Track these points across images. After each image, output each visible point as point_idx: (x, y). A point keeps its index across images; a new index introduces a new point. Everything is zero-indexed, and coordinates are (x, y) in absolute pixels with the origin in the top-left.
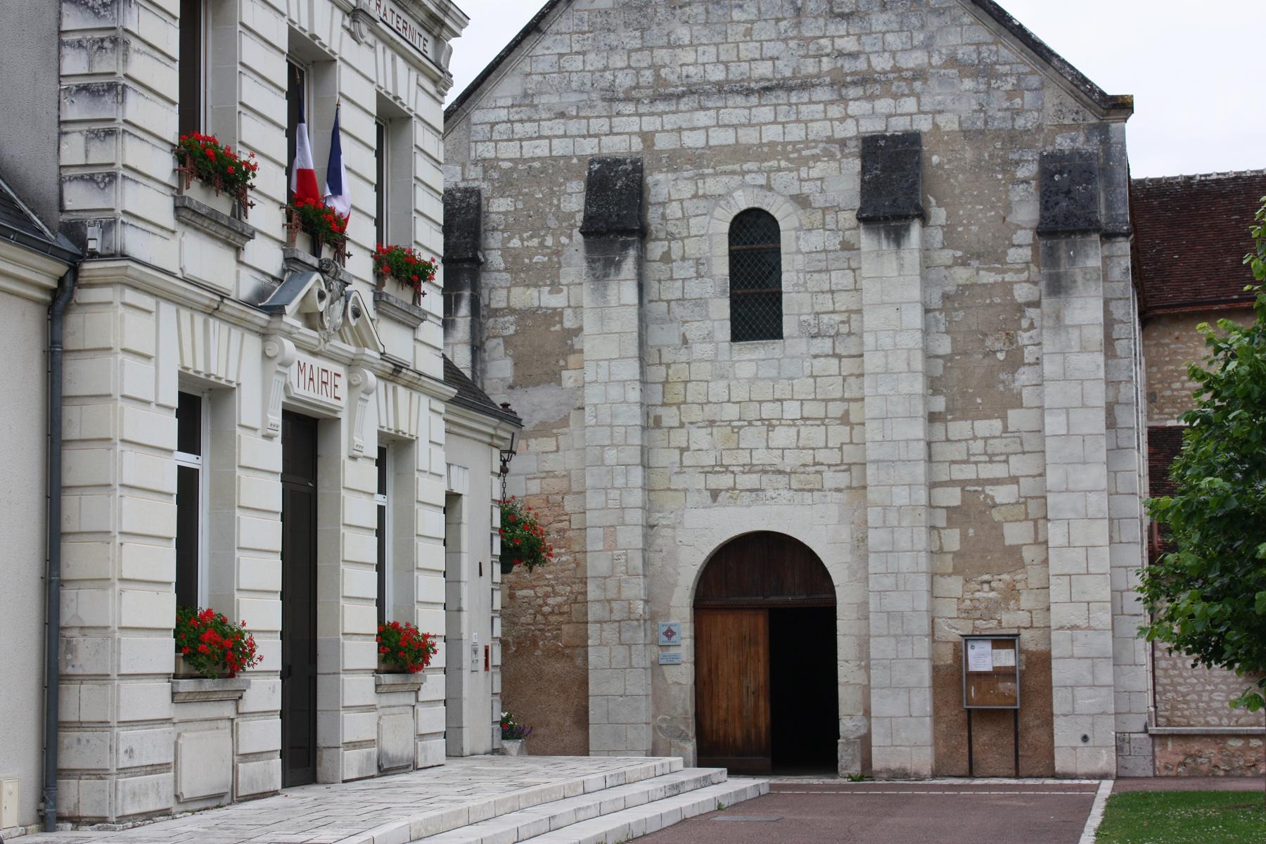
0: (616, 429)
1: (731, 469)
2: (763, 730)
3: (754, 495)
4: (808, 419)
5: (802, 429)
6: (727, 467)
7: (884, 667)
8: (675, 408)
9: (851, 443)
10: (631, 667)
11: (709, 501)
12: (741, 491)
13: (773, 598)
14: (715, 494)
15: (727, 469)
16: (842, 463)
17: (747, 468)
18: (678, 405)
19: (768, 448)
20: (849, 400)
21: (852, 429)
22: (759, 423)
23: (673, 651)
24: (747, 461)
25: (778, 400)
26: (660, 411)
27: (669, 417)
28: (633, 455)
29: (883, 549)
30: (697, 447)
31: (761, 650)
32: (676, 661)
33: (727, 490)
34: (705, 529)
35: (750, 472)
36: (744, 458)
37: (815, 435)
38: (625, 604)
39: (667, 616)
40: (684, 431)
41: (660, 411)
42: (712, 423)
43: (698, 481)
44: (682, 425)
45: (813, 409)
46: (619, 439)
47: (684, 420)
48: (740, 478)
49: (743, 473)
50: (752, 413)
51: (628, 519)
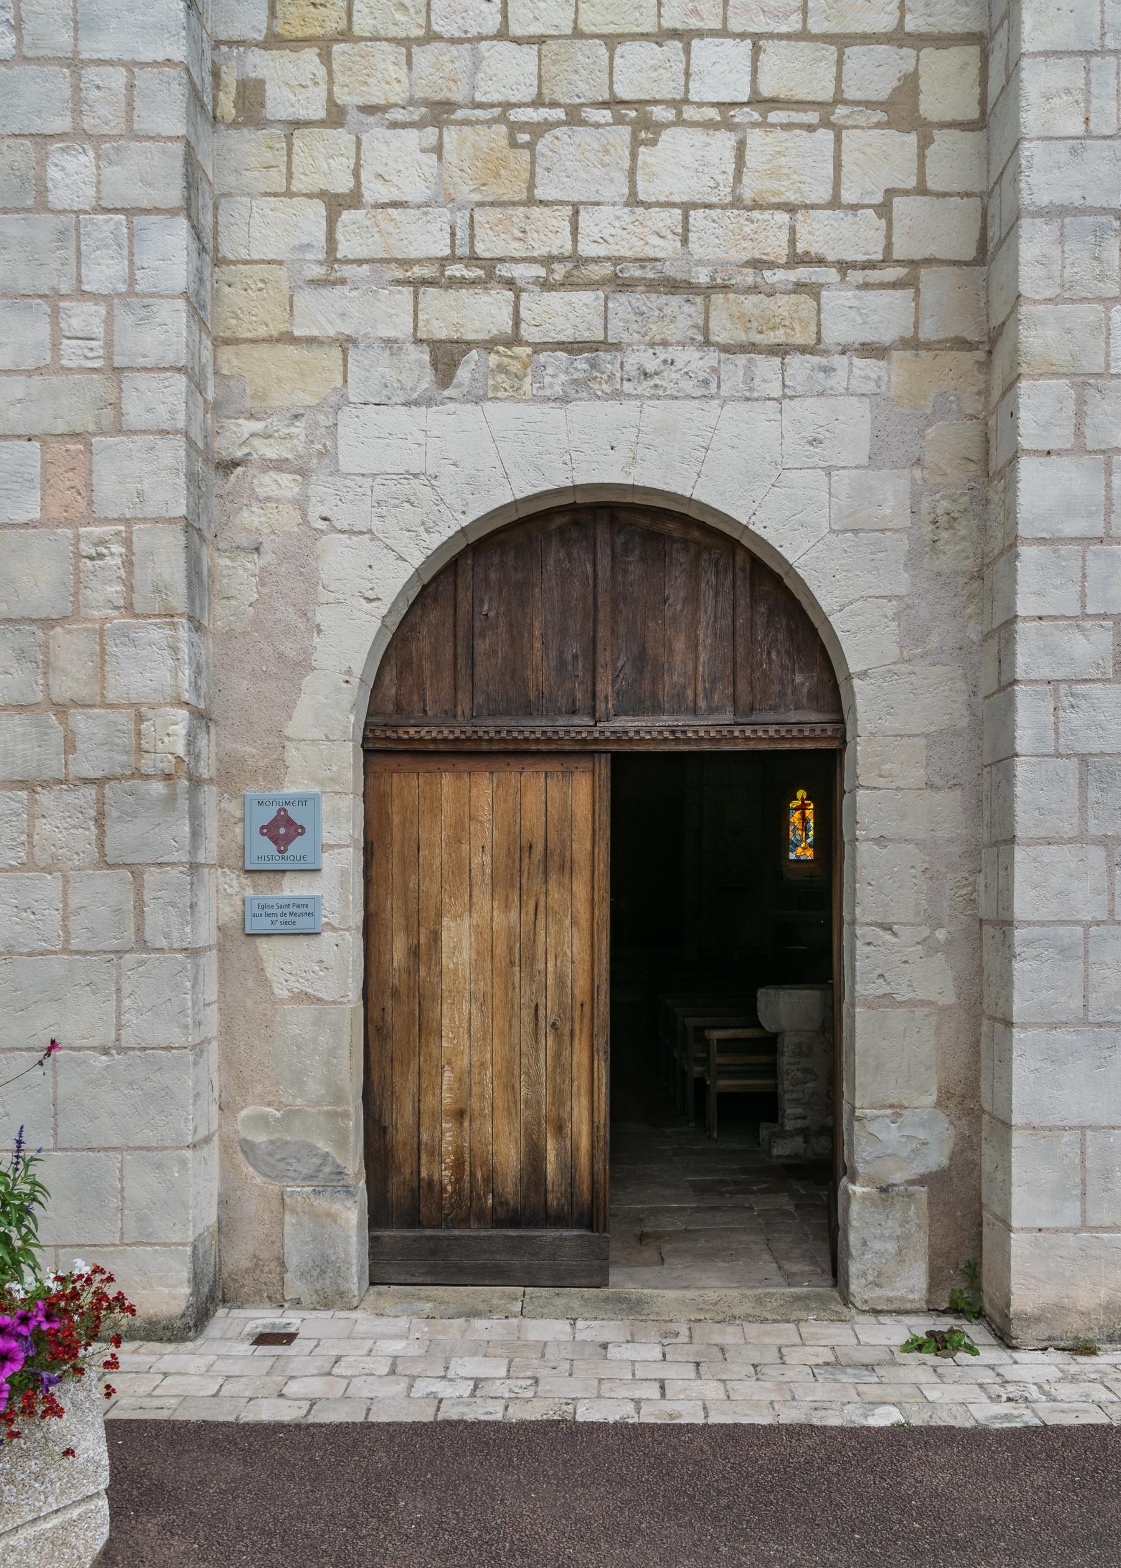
0: (91, 74)
1: (503, 270)
2: (584, 1143)
3: (581, 362)
4: (774, 103)
5: (755, 138)
6: (490, 264)
7: (1064, 951)
8: (310, 56)
9: (922, 190)
10: (143, 945)
11: (427, 381)
12: (539, 348)
13: (622, 723)
14: (446, 357)
15: (489, 273)
16: (887, 260)
17: (560, 271)
18: (324, 45)
19: (634, 201)
20: (919, 41)
21: (925, 142)
22: (605, 116)
23: (293, 888)
24: (561, 243)
25: (674, 34)
26: (263, 65)
27: (292, 84)
28: (152, 175)
29: (1071, 528)
30: (385, 194)
31: (581, 889)
32: (303, 924)
33: (489, 345)
34: (409, 475)
35: (569, 284)
36: (550, 234)
37: (791, 160)
38: (123, 719)
39: (276, 770)
40: (342, 138)
41: (263, 65)
42: (439, 112)
43: (392, 312)
44: (336, 116)
45: (794, 72)
46: (103, 113)
47: (342, 97)
48: (535, 306)
49: (546, 285)
50: (581, 76)
51: (134, 412)
